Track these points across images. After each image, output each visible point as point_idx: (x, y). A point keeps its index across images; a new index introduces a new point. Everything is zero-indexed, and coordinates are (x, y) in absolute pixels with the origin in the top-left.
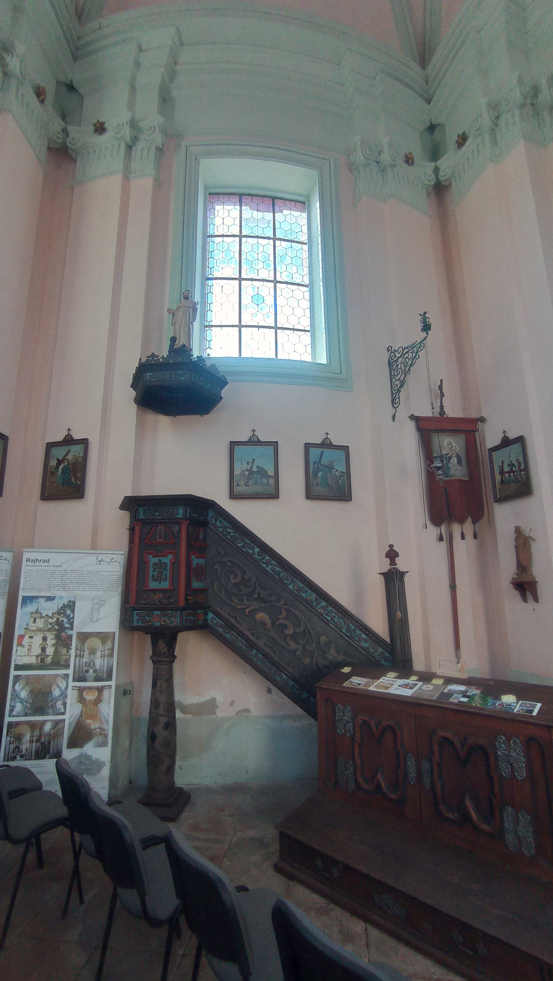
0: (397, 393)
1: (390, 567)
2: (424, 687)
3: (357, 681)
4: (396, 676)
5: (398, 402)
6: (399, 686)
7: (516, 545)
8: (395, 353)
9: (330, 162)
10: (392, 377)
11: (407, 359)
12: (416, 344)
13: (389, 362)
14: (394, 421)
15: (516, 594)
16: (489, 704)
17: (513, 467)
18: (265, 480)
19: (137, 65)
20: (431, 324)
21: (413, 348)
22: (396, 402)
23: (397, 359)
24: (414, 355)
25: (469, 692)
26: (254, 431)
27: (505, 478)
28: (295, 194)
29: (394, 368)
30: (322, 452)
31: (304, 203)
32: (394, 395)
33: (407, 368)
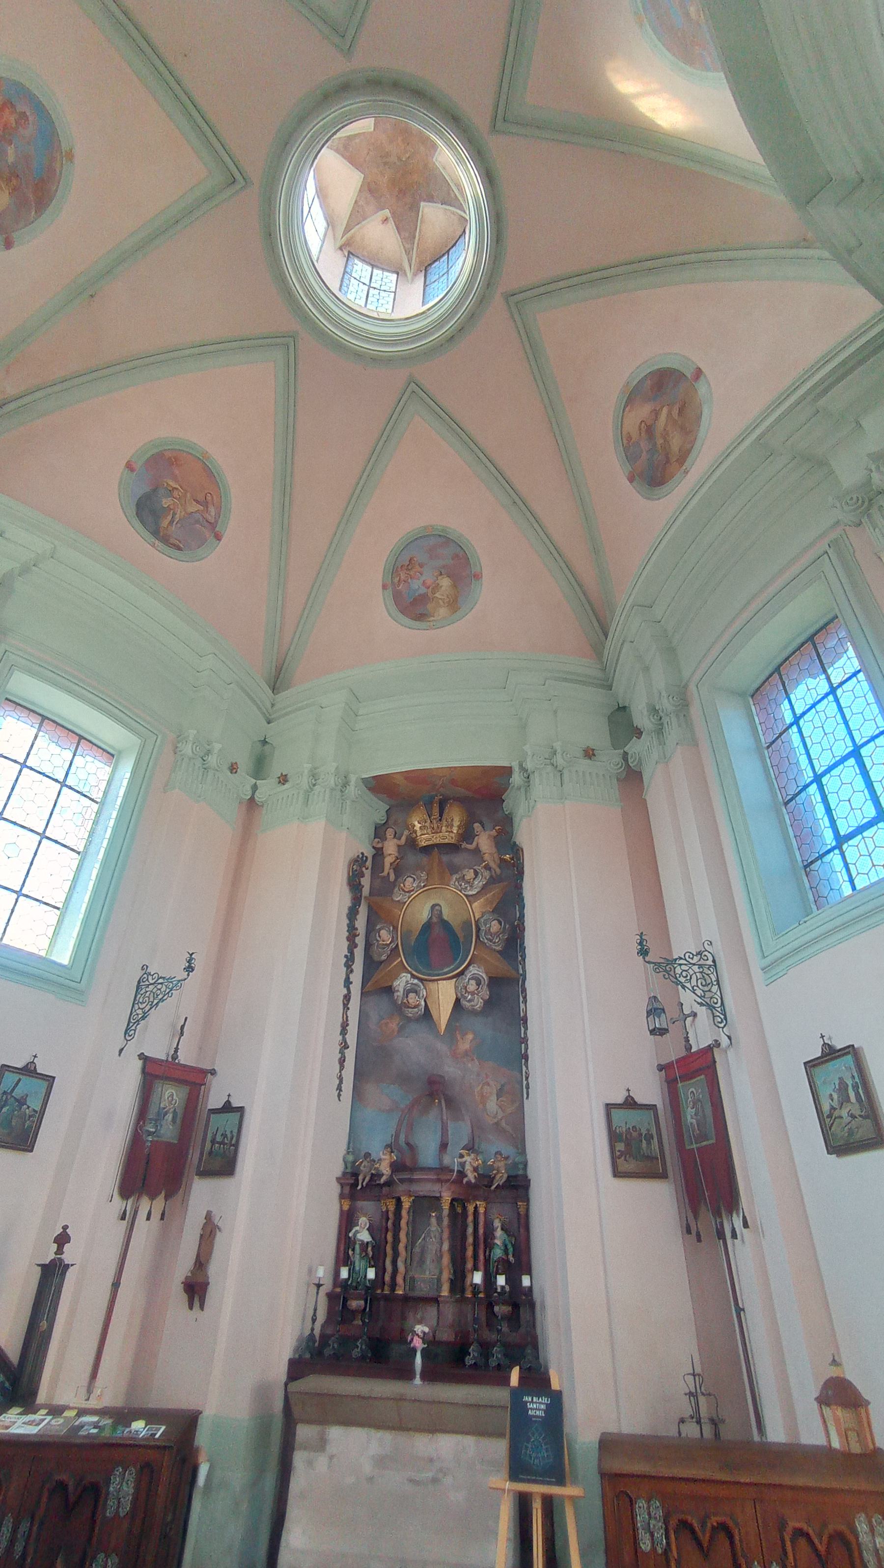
0: (135, 1023)
2: (53, 1422)
4: (21, 1412)
6: (23, 1423)
10: (136, 1002)
11: (159, 991)
13: (139, 982)
15: (185, 1297)
22: (130, 1034)
23: (149, 985)
24: (168, 990)
28: (105, 743)
29: (142, 992)
30: (19, 1080)
32: (131, 1024)
33: (155, 1002)
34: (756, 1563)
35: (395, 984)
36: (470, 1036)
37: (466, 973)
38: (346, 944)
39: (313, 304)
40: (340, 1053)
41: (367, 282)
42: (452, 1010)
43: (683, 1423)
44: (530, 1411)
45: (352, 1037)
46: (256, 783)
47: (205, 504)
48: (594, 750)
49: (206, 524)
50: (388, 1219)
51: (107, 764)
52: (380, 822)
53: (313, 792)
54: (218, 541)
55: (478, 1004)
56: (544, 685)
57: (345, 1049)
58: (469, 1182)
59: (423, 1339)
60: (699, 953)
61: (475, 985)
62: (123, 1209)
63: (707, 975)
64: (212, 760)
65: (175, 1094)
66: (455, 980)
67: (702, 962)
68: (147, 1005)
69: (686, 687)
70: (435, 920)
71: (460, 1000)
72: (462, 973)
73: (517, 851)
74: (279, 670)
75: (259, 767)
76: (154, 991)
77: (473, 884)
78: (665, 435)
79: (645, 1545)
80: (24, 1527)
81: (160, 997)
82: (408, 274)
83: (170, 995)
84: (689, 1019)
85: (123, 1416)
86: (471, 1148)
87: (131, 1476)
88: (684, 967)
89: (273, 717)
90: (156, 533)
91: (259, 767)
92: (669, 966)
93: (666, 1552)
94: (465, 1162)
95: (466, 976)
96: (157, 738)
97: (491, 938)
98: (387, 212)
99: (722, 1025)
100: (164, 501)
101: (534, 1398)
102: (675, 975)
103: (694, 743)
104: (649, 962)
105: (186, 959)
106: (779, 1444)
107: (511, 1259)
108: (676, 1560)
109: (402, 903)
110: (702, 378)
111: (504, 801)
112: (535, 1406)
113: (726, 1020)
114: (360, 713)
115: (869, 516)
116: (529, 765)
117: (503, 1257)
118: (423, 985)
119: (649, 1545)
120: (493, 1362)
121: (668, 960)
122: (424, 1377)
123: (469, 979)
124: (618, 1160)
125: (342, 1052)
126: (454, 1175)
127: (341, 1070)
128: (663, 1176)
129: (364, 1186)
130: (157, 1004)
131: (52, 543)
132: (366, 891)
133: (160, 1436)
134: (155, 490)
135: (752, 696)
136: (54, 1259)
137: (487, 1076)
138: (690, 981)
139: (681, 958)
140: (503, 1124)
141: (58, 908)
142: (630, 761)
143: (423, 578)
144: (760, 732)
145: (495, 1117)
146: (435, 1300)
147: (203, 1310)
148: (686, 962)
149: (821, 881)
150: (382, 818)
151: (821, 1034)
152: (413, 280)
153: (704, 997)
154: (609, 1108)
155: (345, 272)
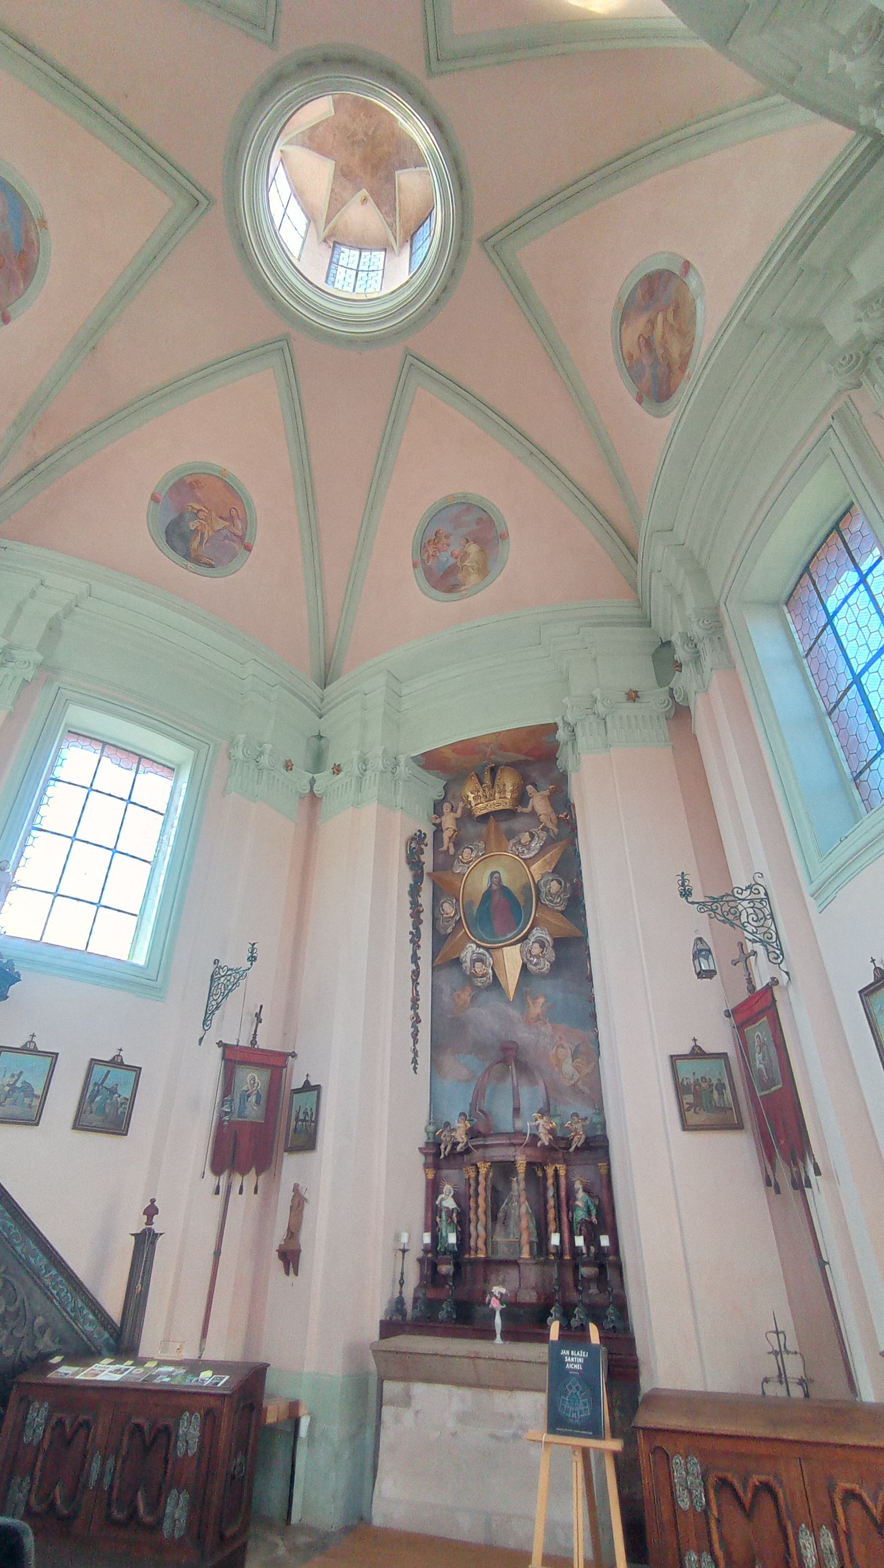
1: (145, 1227)
3: (67, 1372)
12: (240, 970)
13: (212, 976)
14: (200, 1044)
15: (281, 1263)
18: (27, 1100)
19: (33, 594)
24: (236, 980)
26: (33, 1036)
28: (165, 759)
30: (109, 1071)
32: (208, 1015)
33: (226, 992)
34: (803, 1526)
36: (541, 1000)
37: (529, 937)
38: (411, 920)
39: (298, 302)
40: (412, 1027)
41: (370, 269)
42: (520, 976)
43: (767, 1383)
44: (568, 1365)
45: (425, 1012)
46: (313, 777)
47: (231, 519)
48: (637, 691)
49: (234, 538)
52: (438, 799)
53: (365, 778)
54: (248, 553)
55: (545, 966)
56: (578, 634)
57: (417, 1023)
58: (543, 1145)
60: (749, 887)
61: (539, 947)
62: (217, 1184)
63: (759, 909)
64: (265, 760)
67: (752, 896)
69: (717, 607)
70: (495, 887)
72: (525, 937)
73: (569, 807)
74: (328, 666)
75: (318, 761)
76: (225, 983)
79: (684, 1503)
80: (110, 1462)
82: (395, 247)
84: (752, 958)
85: (195, 1367)
86: (545, 1112)
88: (732, 904)
89: (322, 711)
90: (187, 556)
91: (318, 761)
92: (715, 904)
93: (706, 1511)
94: (539, 1125)
95: (530, 940)
96: (209, 747)
97: (553, 899)
98: (364, 192)
99: (779, 961)
100: (191, 524)
101: (572, 1352)
103: (731, 665)
104: (693, 903)
106: (871, 1404)
107: (594, 1220)
108: (844, 1532)
110: (691, 272)
111: (558, 759)
112: (572, 1359)
113: (783, 955)
114: (403, 693)
115: (868, 374)
116: (570, 718)
117: (587, 1219)
119: (688, 1503)
121: (714, 898)
122: (506, 1335)
123: (533, 942)
128: (738, 1126)
129: (447, 1155)
131: (87, 583)
132: (428, 867)
133: (222, 1385)
134: (181, 516)
135: (786, 604)
136: (144, 1230)
137: (560, 1038)
139: (728, 895)
141: (135, 915)
142: (676, 696)
144: (797, 640)
146: (515, 1263)
147: (297, 1275)
148: (734, 899)
149: (872, 791)
150: (440, 794)
151: (872, 958)
152: (400, 252)
153: (756, 933)
154: (674, 1059)
155: (331, 262)
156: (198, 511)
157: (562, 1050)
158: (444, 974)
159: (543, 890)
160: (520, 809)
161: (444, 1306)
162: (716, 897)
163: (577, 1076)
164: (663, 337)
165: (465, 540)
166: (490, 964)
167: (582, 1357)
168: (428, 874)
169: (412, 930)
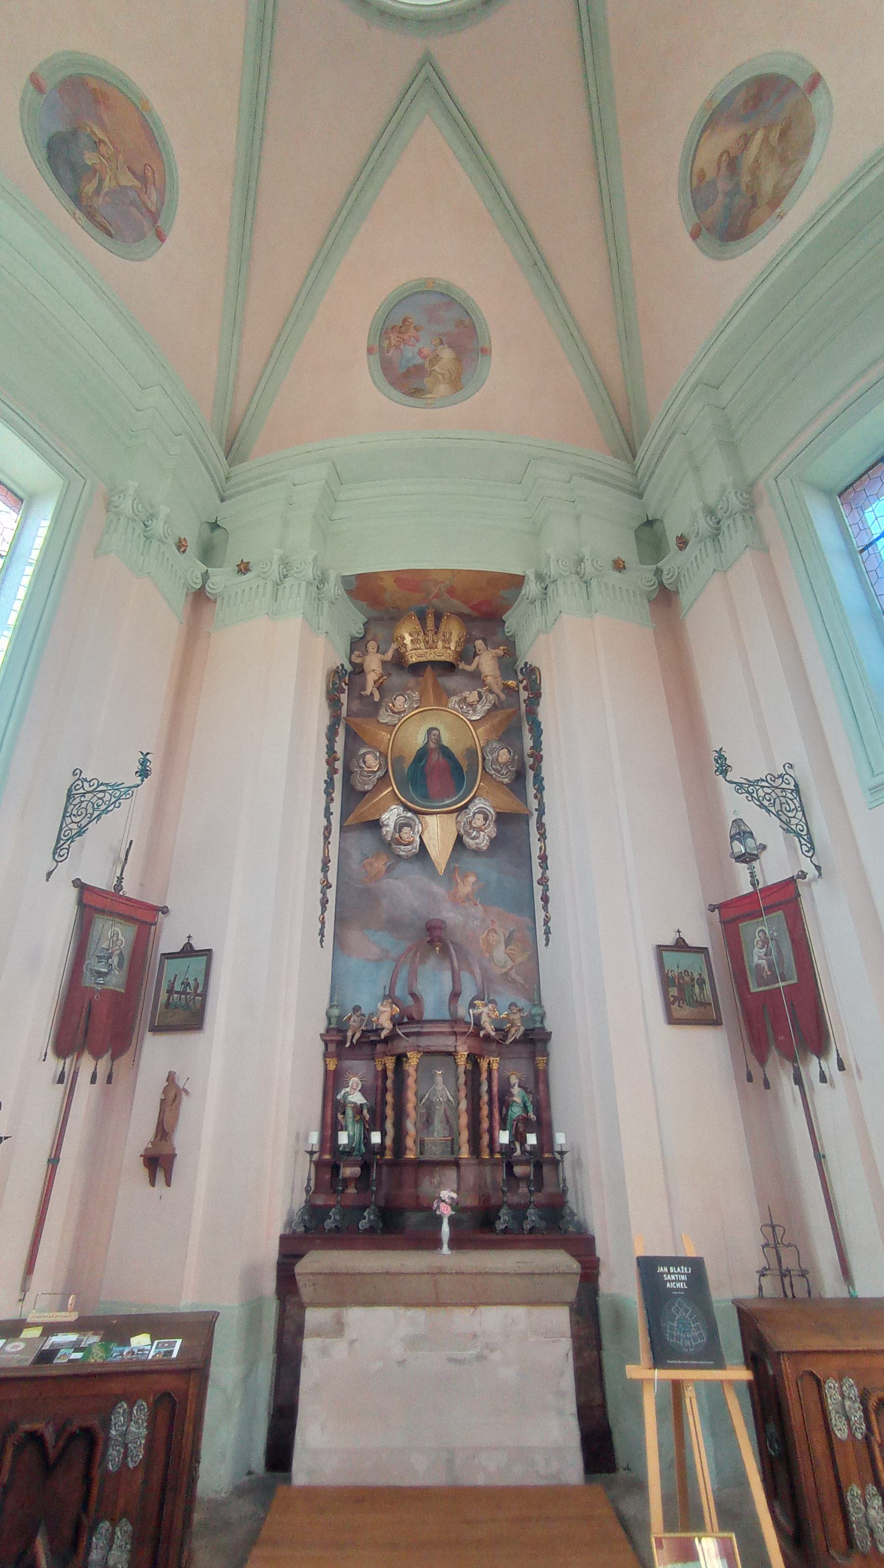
5: (64, 855)
7: (163, 1098)
8: (85, 783)
9: (85, 483)
10: (68, 815)
11: (101, 801)
12: (121, 786)
13: (70, 790)
14: (47, 880)
15: (144, 1172)
16: (114, 1355)
17: (188, 987)
20: (150, 771)
21: (116, 789)
24: (113, 800)
25: (83, 1343)
27: (173, 999)
31: (22, 500)
32: (62, 842)
33: (96, 813)
35: (385, 817)
36: (472, 879)
37: (470, 807)
44: (668, 1283)
50: (385, 1078)
51: (13, 508)
53: (283, 586)
54: (160, 243)
55: (483, 842)
59: (451, 1205)
62: (61, 1069)
63: (791, 800)
65: (120, 932)
66: (456, 814)
67: (784, 786)
68: (84, 818)
70: (432, 745)
71: (462, 837)
72: (465, 806)
77: (476, 708)
78: (755, 171)
79: (841, 1432)
81: (103, 807)
83: (117, 805)
87: (141, 1411)
90: (77, 198)
94: (480, 1014)
99: (810, 854)
101: (671, 1268)
102: (758, 798)
103: (764, 548)
104: (730, 782)
105: (139, 761)
107: (533, 1116)
109: (391, 725)
110: (820, 86)
111: (505, 622)
117: (523, 1115)
118: (418, 819)
120: (527, 1226)
122: (457, 1243)
123: (475, 814)
124: (672, 1006)
125: (324, 893)
126: (471, 1028)
127: (323, 912)
128: (716, 1022)
130: (99, 816)
134: (75, 132)
135: (840, 496)
138: (774, 806)
139: (763, 780)
140: (513, 974)
143: (419, 345)
145: (503, 967)
150: (360, 631)
154: (661, 949)
156: (101, 141)
157: (495, 935)
158: (353, 837)
159: (489, 757)
160: (462, 666)
161: (365, 1214)
162: (751, 780)
163: (510, 964)
164: (756, 160)
165: (438, 341)
166: (418, 831)
167: (684, 1274)
168: (344, 718)
169: (326, 779)
